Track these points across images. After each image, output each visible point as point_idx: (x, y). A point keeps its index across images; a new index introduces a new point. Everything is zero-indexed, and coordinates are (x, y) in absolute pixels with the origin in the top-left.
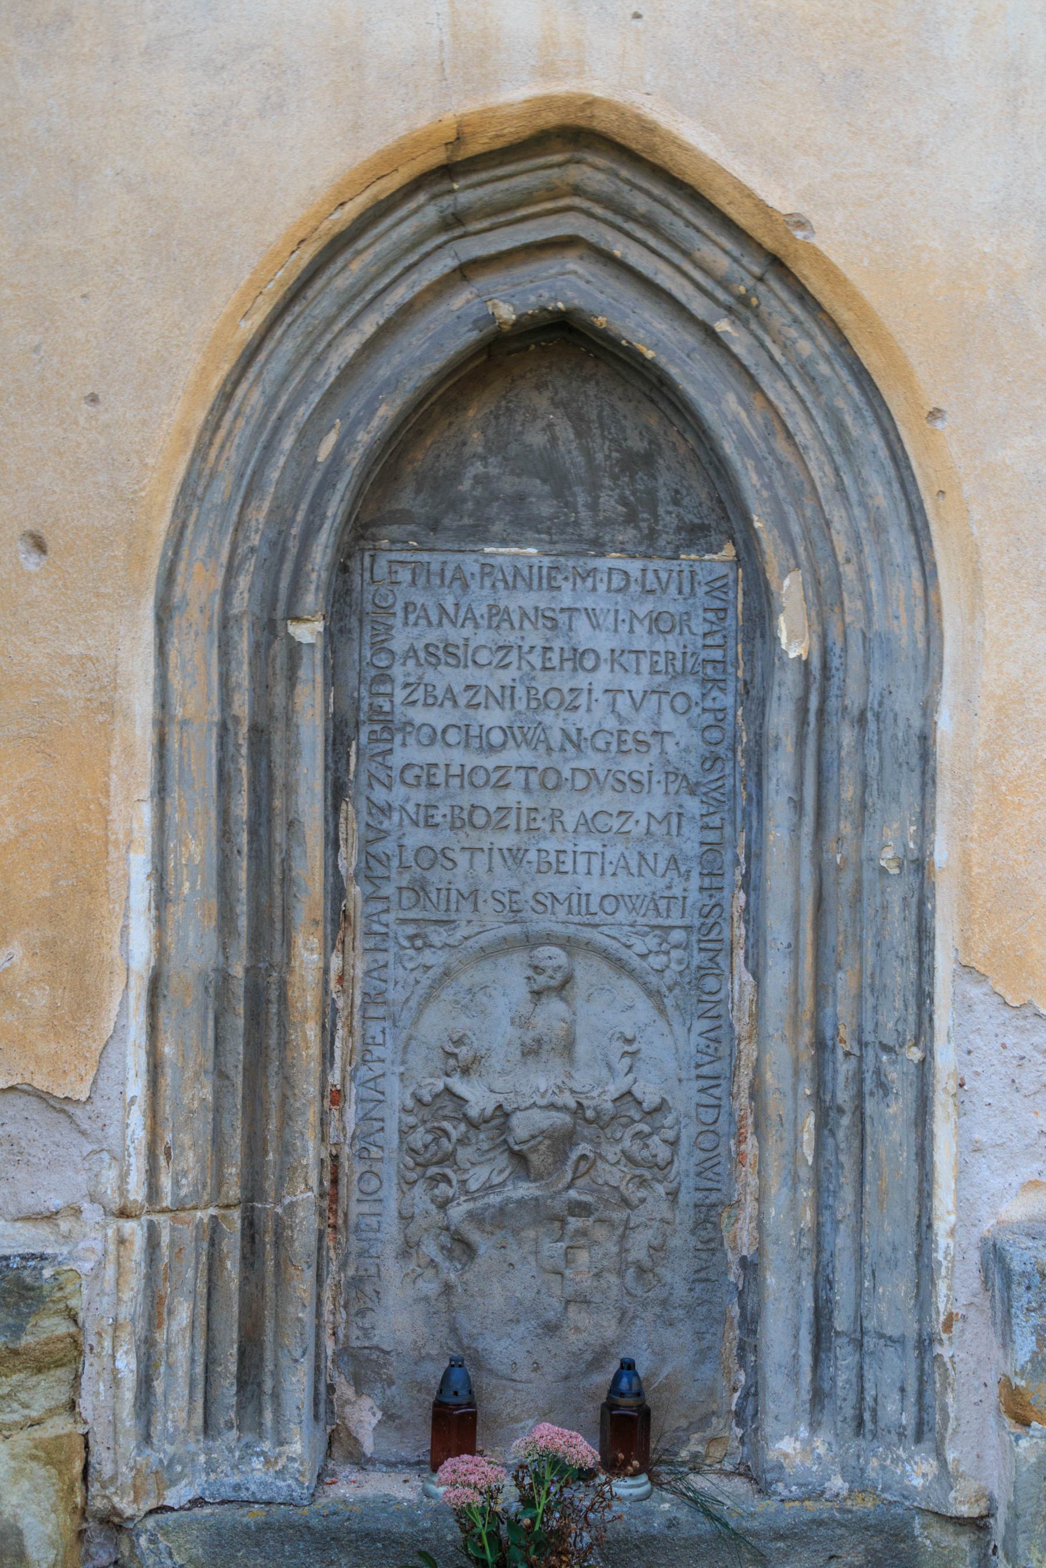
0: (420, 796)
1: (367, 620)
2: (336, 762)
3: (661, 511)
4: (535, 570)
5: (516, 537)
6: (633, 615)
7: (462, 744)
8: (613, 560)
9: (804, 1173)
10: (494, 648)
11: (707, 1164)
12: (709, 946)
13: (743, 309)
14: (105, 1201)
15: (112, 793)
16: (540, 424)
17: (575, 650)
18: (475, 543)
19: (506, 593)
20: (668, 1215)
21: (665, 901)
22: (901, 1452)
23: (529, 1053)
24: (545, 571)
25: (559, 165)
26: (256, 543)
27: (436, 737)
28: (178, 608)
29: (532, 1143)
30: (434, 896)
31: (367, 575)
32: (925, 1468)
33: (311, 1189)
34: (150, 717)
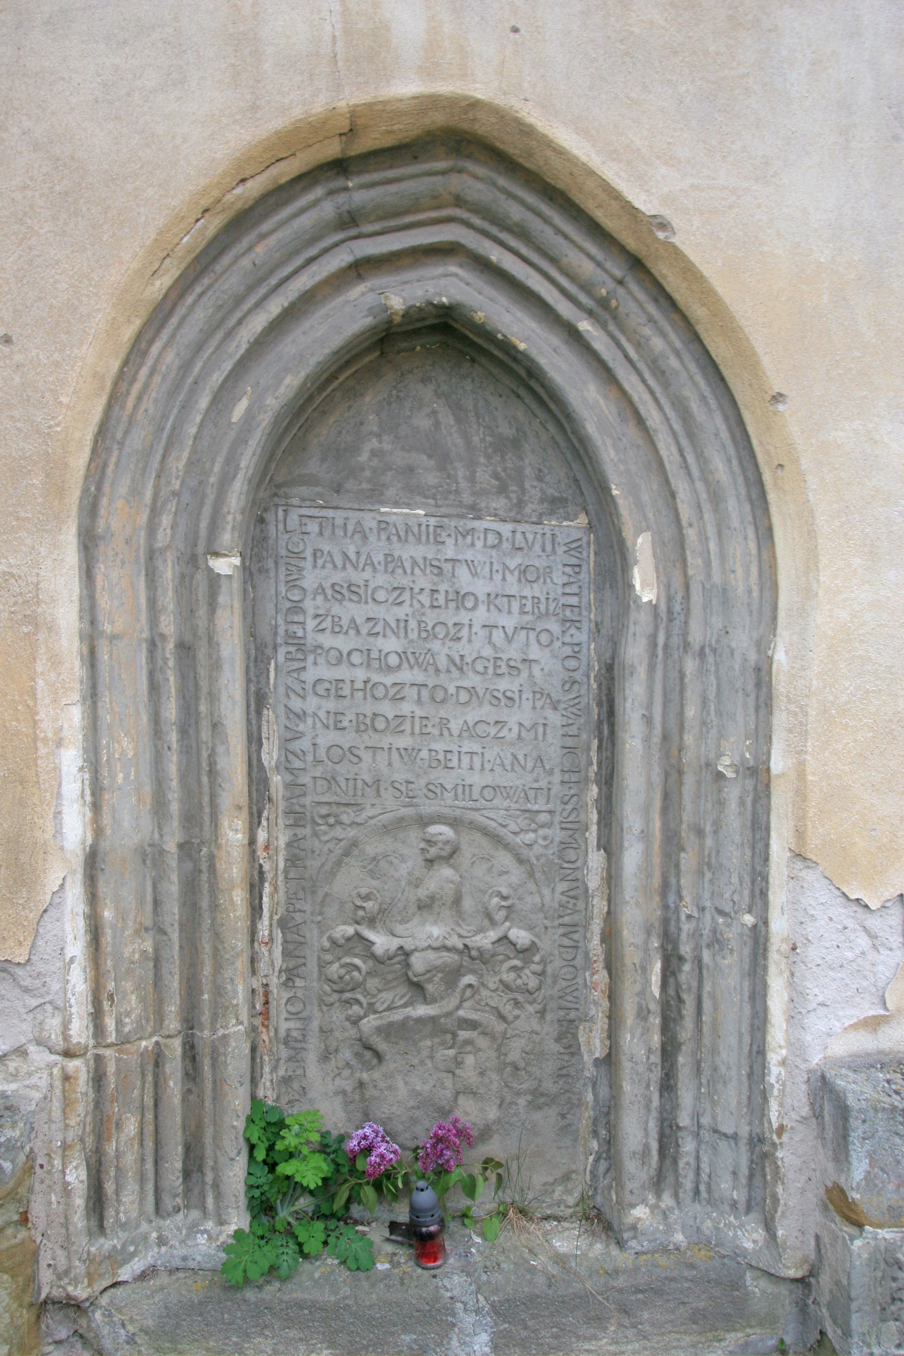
0: (331, 705)
1: (282, 562)
2: (257, 677)
3: (527, 485)
4: (423, 528)
5: (407, 501)
6: (506, 567)
7: (365, 664)
8: (488, 523)
9: (654, 1007)
10: (390, 588)
11: (568, 991)
12: (569, 826)
13: (603, 310)
14: (51, 1044)
15: (39, 696)
16: (426, 411)
17: (458, 593)
18: (373, 504)
19: (399, 545)
20: (537, 1028)
21: (533, 792)
22: (732, 1218)
23: (424, 907)
24: (431, 529)
25: (443, 173)
26: (177, 487)
28: (103, 538)
29: (428, 975)
30: (343, 784)
31: (281, 526)
32: (755, 1236)
33: (241, 1023)
34: (75, 631)
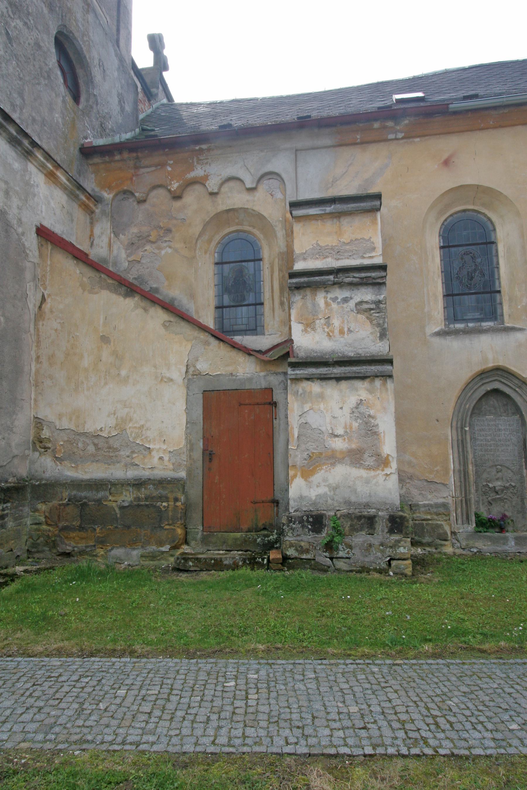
8: (503, 417)
13: (520, 387)
27: (481, 440)
